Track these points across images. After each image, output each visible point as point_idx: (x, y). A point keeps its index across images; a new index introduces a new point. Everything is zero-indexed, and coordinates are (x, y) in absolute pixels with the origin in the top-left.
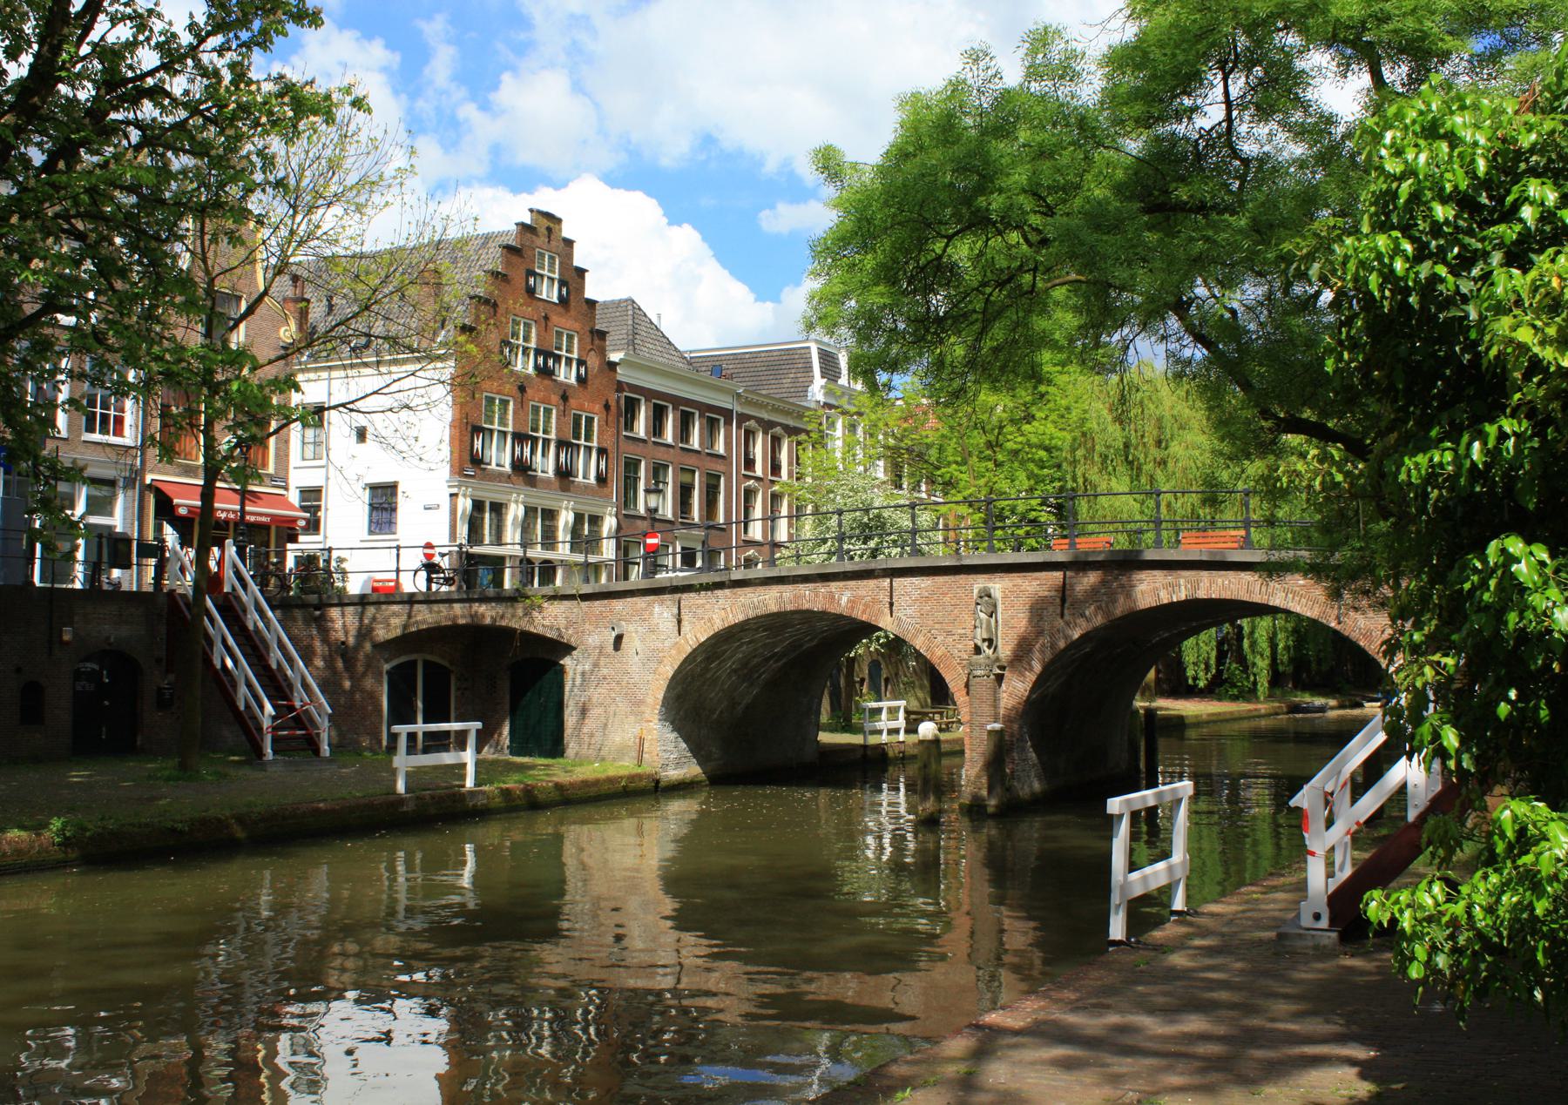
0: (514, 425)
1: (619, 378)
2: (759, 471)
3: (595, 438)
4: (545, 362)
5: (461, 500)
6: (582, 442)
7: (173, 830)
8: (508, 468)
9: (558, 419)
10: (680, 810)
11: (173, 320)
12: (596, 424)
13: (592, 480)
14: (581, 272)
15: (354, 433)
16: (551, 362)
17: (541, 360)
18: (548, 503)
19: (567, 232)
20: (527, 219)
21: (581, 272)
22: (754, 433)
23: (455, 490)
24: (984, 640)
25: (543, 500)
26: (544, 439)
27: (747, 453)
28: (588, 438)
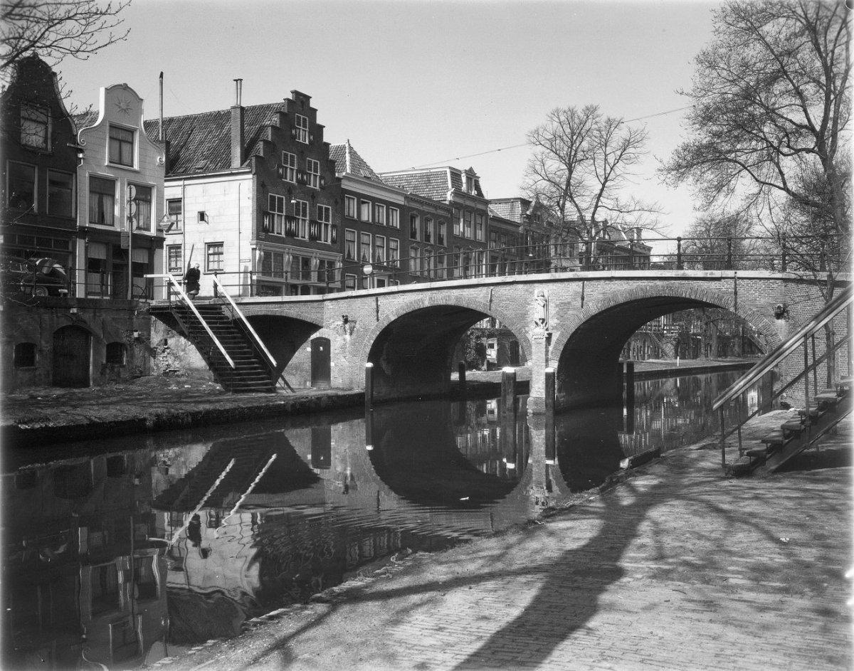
0: (286, 212)
1: (343, 186)
2: (418, 239)
3: (330, 220)
4: (302, 177)
5: (258, 252)
6: (323, 222)
7: (498, 632)
8: (283, 235)
9: (310, 209)
10: (287, 378)
11: (149, 148)
12: (330, 212)
13: (329, 242)
14: (321, 127)
15: (206, 218)
16: (305, 177)
17: (300, 176)
18: (306, 254)
19: (313, 104)
20: (290, 97)
21: (321, 127)
22: (415, 218)
23: (254, 247)
24: (540, 319)
25: (303, 252)
26: (325, 224)
27: (426, 232)
28: (327, 219)
